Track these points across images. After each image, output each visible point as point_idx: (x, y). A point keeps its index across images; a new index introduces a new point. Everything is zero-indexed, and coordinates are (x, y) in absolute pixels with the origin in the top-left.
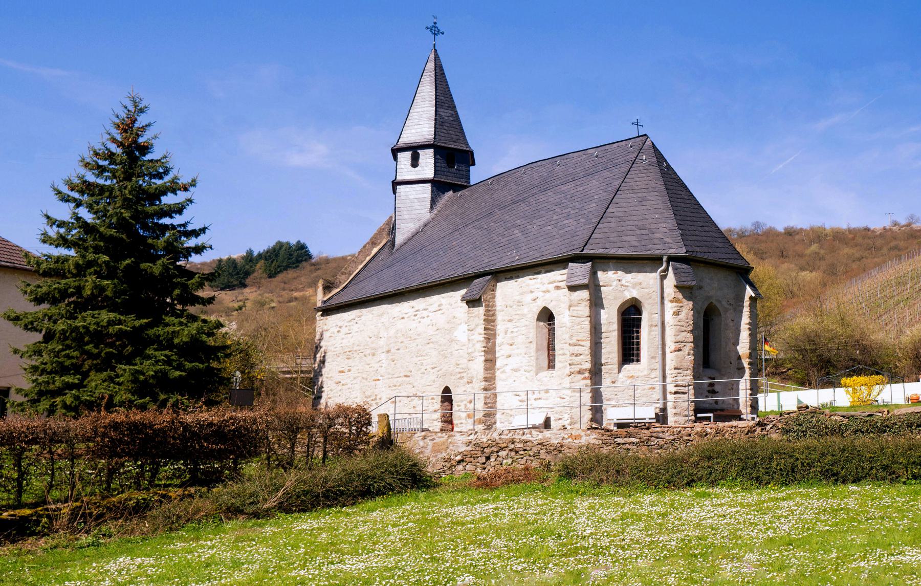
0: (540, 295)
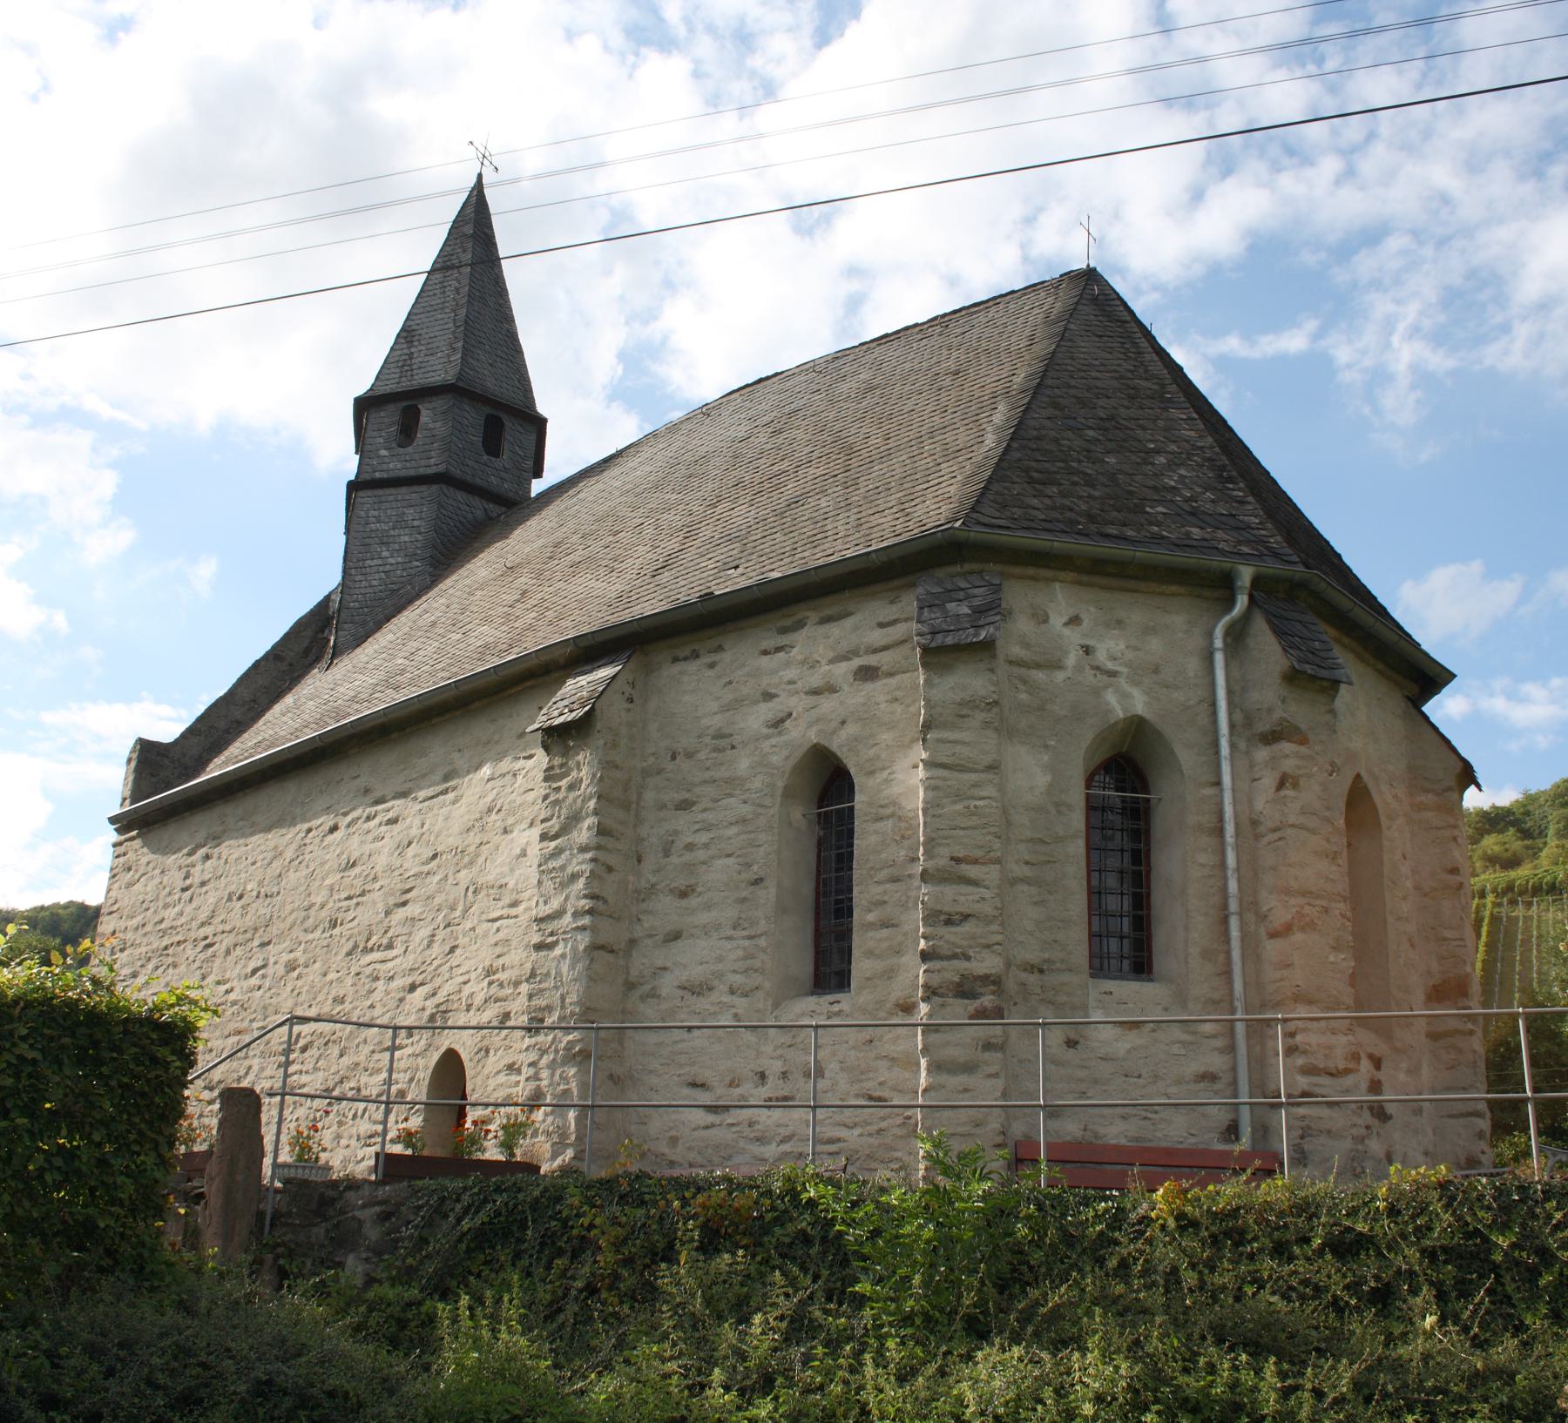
0: (797, 703)
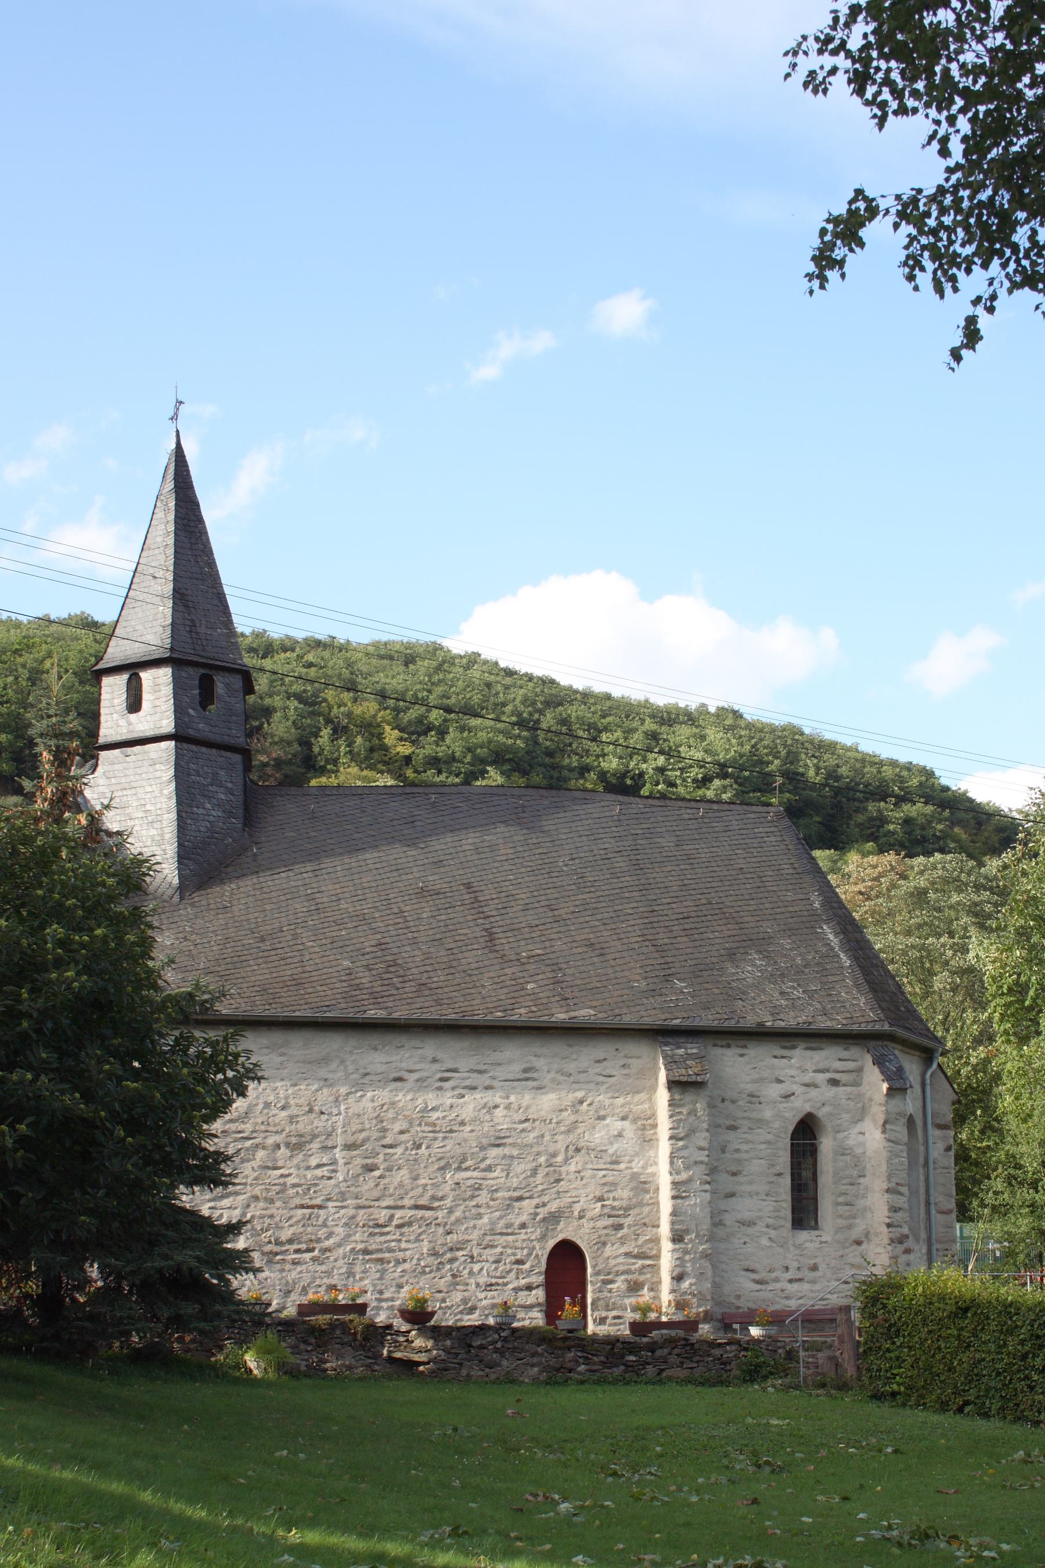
0: (798, 1089)
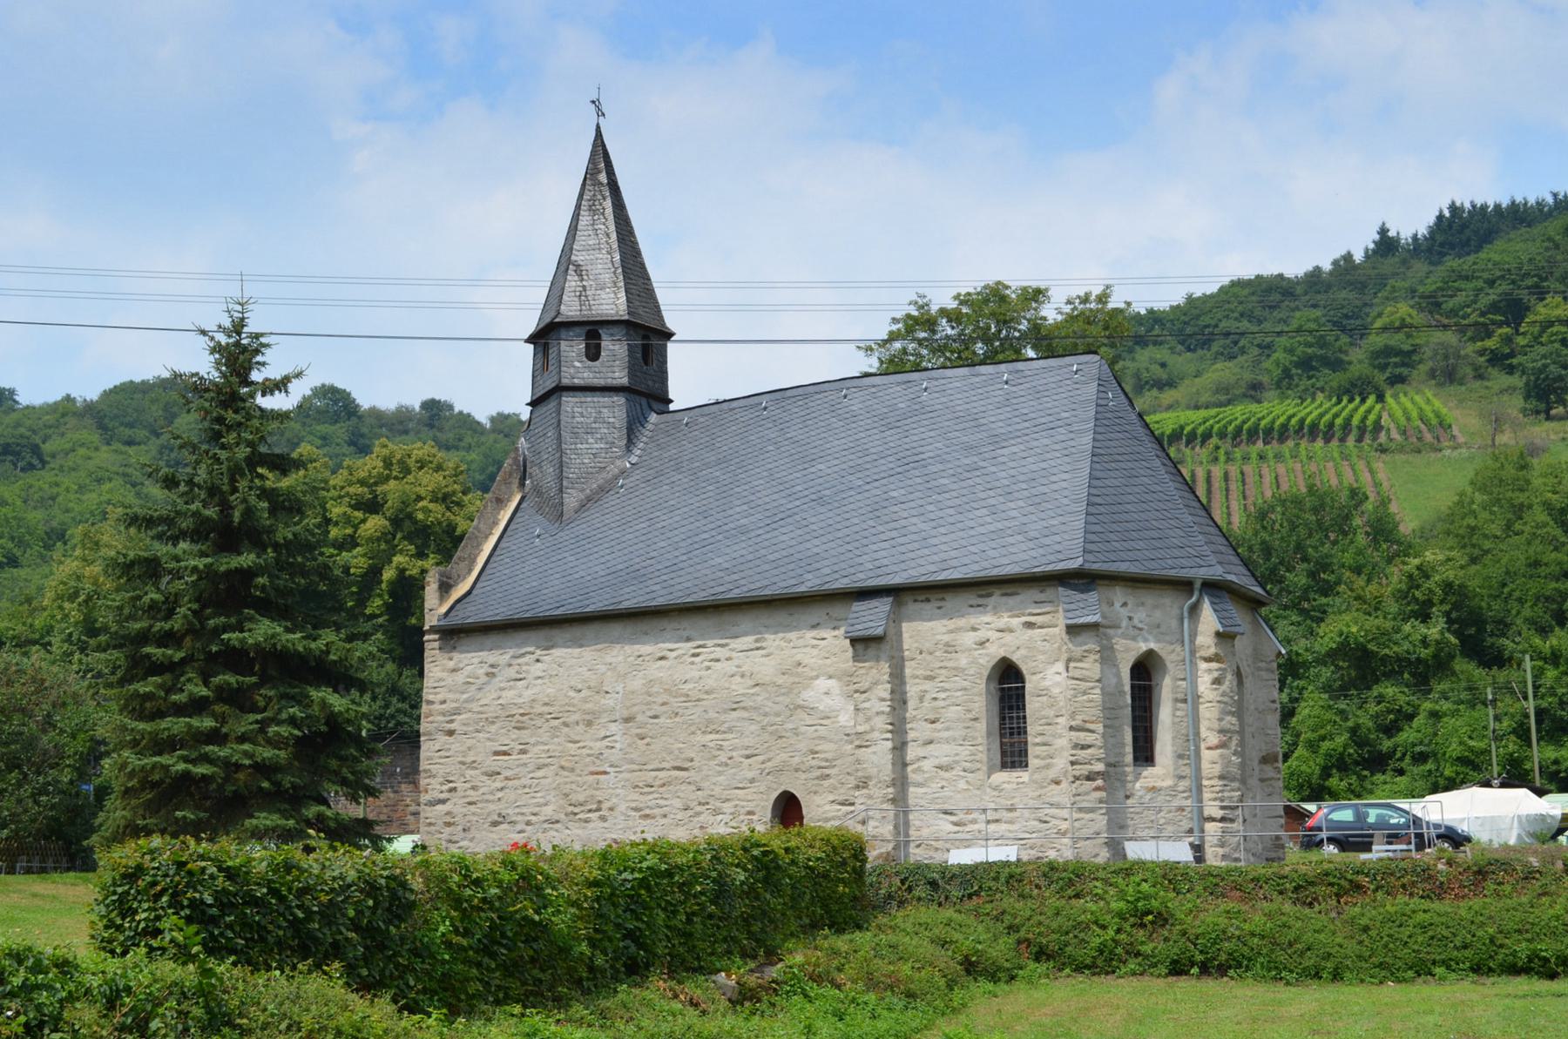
0: (993, 635)
